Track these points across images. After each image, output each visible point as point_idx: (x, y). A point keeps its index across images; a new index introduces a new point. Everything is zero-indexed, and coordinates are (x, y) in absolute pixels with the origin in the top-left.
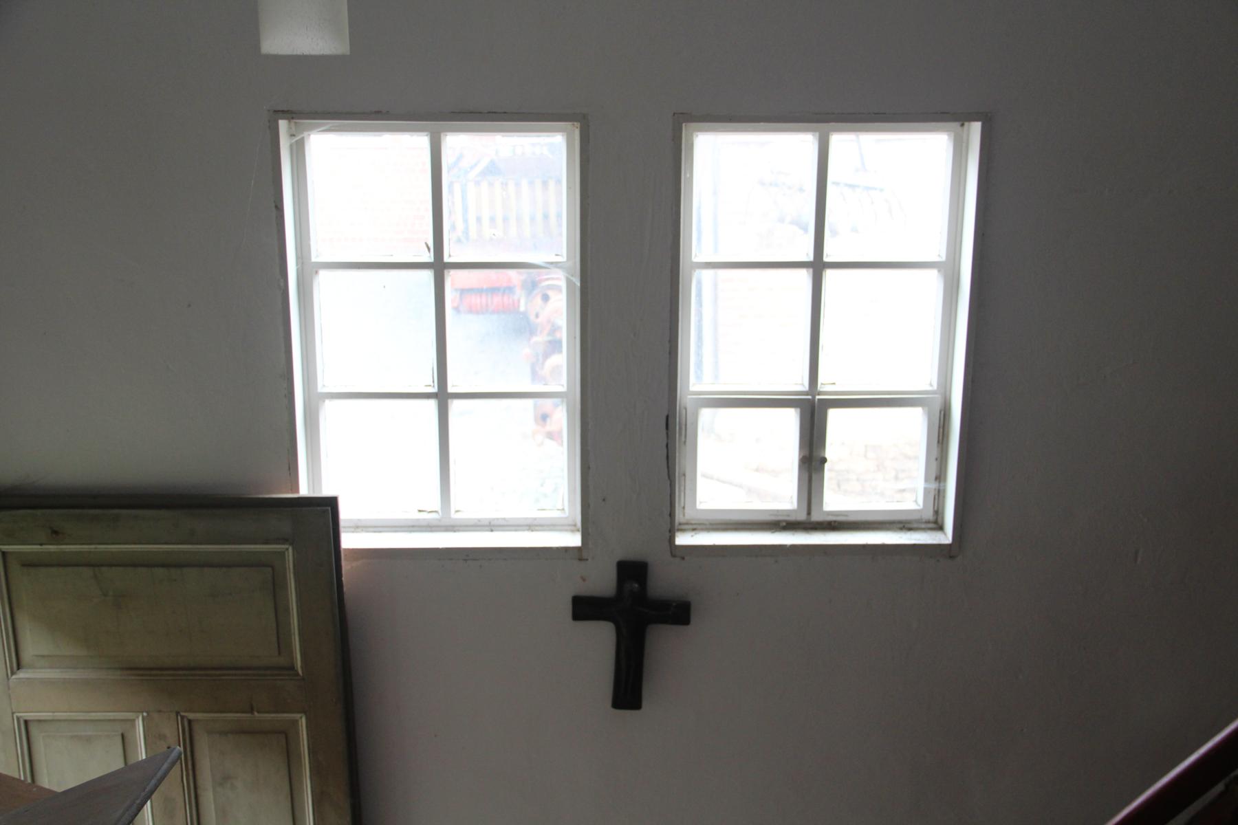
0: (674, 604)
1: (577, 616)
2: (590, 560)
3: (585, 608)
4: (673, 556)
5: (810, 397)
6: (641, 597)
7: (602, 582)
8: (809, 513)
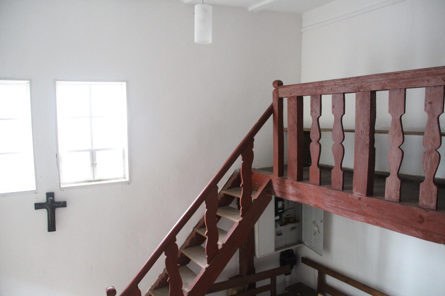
0: (62, 202)
1: (54, 230)
2: (38, 193)
3: (38, 206)
4: (61, 190)
5: (92, 149)
6: (53, 201)
7: (43, 199)
8: (94, 178)
